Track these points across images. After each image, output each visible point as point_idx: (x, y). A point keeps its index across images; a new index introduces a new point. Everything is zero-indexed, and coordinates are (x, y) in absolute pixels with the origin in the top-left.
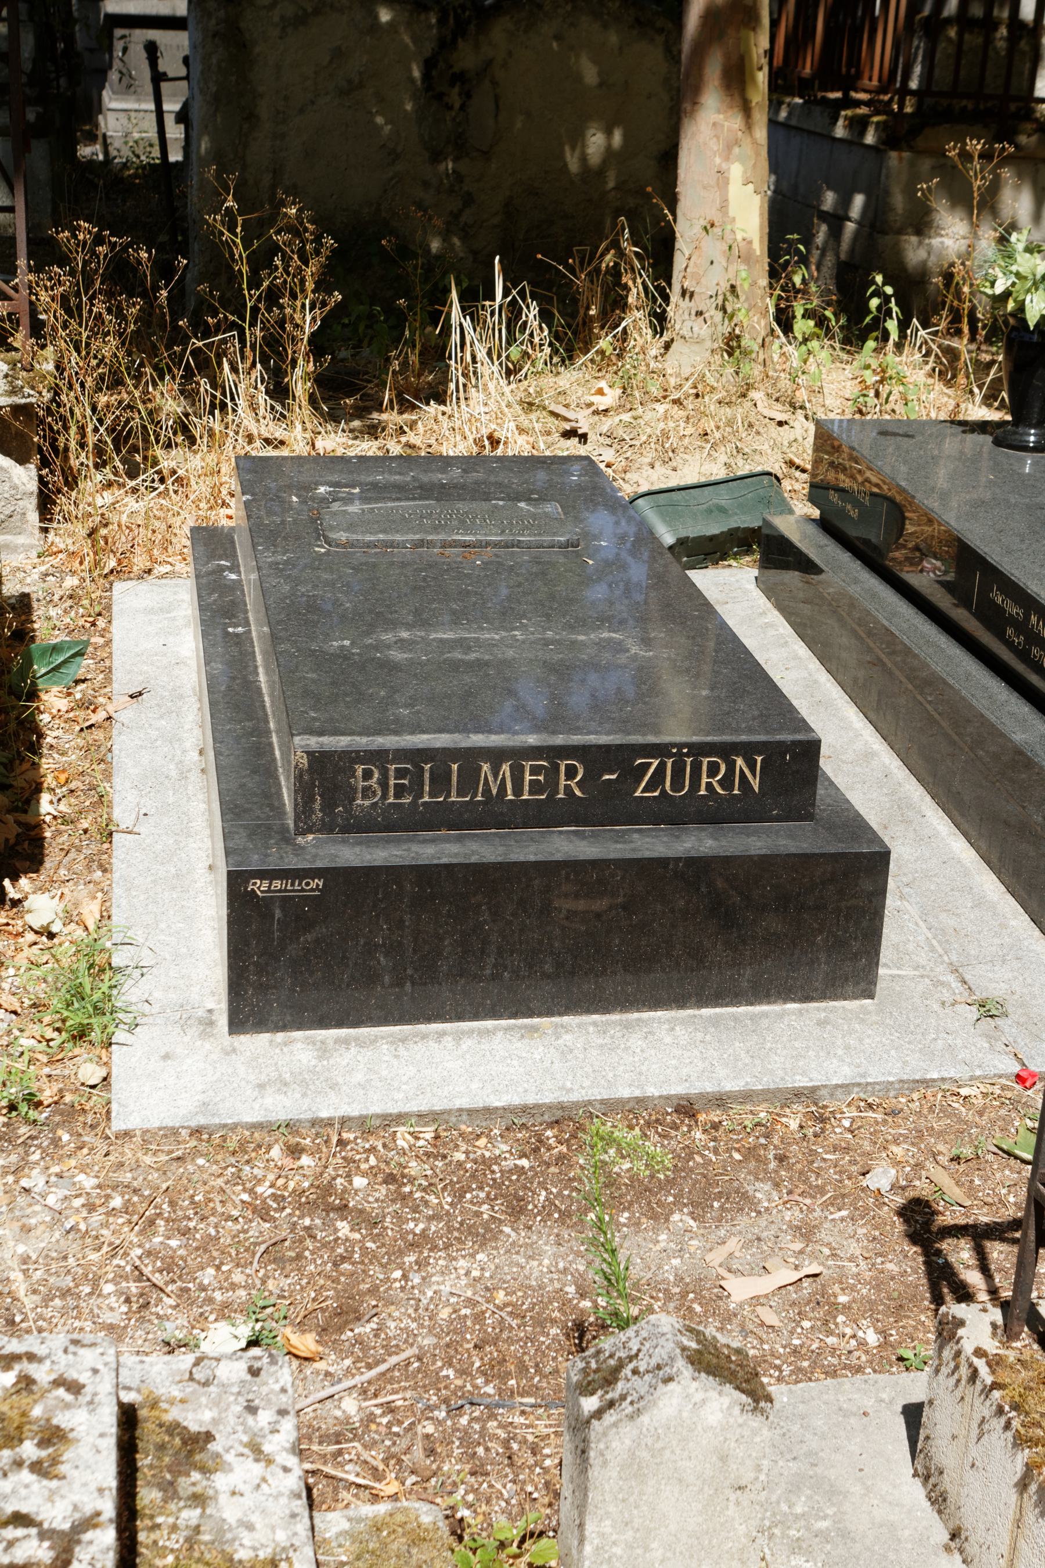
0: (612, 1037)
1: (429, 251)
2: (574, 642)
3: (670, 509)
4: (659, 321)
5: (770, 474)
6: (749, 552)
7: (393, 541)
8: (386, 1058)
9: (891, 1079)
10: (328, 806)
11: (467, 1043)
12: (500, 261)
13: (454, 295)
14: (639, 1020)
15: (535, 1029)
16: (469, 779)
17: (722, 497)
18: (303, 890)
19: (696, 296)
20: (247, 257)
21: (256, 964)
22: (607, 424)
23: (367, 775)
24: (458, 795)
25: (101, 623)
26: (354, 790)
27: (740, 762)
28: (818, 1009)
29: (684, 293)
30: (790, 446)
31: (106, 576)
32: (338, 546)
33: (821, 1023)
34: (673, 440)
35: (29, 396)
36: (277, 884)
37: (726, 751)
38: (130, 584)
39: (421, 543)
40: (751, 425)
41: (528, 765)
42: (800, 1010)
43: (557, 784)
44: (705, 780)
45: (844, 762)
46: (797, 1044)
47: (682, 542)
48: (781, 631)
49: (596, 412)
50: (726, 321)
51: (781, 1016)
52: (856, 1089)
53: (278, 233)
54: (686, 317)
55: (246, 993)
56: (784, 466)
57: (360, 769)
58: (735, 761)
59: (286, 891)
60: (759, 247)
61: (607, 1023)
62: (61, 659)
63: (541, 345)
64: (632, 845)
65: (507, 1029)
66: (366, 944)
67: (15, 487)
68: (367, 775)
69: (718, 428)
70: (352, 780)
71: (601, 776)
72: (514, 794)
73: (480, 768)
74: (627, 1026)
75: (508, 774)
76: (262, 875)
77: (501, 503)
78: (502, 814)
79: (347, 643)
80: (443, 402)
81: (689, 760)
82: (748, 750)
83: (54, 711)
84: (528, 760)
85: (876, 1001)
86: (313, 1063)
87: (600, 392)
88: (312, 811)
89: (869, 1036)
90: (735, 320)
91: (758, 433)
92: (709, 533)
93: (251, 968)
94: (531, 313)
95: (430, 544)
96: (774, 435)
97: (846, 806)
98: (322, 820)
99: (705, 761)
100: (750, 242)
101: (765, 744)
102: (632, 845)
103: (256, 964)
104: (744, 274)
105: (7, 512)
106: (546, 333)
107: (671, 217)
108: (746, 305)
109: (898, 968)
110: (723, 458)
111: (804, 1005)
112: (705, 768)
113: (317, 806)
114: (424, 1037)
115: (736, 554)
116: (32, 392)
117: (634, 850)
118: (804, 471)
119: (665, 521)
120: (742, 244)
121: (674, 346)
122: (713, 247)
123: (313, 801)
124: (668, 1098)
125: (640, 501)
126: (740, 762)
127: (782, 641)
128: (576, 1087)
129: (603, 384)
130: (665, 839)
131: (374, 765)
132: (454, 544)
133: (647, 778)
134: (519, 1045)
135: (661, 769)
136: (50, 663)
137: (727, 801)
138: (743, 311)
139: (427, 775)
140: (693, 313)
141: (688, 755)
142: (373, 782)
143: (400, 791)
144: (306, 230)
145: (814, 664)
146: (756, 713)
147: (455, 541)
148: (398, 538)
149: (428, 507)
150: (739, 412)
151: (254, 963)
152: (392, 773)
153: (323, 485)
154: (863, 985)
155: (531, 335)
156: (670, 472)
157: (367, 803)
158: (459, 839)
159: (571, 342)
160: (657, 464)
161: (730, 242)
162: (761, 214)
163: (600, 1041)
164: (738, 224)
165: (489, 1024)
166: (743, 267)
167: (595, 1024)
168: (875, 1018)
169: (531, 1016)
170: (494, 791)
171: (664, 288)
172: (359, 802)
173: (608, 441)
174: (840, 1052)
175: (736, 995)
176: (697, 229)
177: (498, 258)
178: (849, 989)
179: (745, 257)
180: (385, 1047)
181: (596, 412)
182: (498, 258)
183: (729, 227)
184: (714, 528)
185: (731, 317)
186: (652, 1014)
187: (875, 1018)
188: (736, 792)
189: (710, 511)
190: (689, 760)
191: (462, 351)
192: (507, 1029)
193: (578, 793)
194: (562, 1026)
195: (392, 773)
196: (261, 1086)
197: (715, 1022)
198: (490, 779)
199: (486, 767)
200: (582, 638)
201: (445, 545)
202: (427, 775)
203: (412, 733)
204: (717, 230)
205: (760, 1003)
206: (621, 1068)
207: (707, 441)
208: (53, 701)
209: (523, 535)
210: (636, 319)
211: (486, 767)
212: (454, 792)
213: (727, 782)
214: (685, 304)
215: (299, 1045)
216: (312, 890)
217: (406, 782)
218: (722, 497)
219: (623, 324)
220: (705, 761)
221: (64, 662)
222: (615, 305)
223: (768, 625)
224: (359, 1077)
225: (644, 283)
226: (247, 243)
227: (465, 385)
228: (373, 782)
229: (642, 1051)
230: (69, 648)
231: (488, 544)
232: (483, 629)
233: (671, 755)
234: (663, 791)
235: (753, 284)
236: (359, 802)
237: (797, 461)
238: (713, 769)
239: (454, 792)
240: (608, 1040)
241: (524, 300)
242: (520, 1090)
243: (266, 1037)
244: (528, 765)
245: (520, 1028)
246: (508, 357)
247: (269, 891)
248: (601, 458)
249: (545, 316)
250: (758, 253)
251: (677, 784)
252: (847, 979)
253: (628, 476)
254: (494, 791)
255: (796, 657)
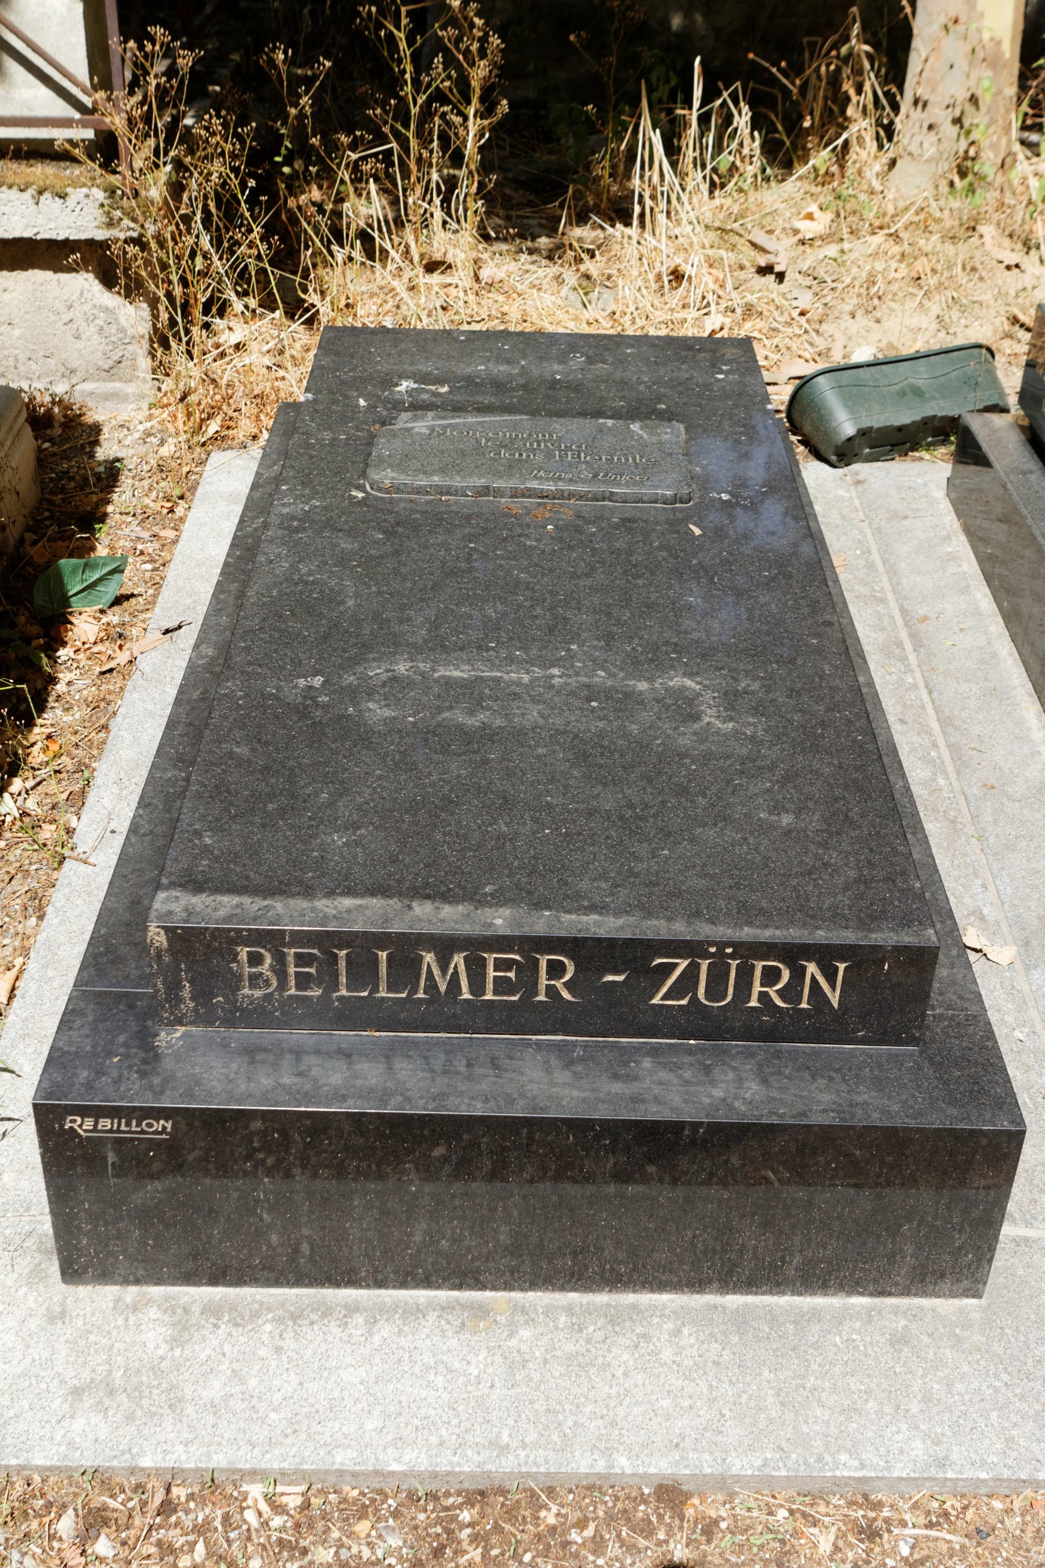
0: (588, 1341)
1: (669, 27)
2: (628, 695)
3: (854, 390)
4: (887, 132)
5: (980, 346)
6: (945, 442)
7: (450, 487)
8: (263, 1352)
9: (983, 1475)
10: (202, 996)
11: (385, 1330)
12: (702, 63)
13: (644, 103)
14: (634, 1307)
15: (482, 1311)
16: (405, 968)
17: (920, 376)
18: (143, 1132)
19: (929, 106)
20: (412, 55)
21: (88, 1212)
22: (811, 258)
23: (255, 960)
24: (389, 990)
25: (180, 511)
26: (240, 978)
27: (812, 968)
28: (896, 1310)
29: (916, 102)
30: (1017, 296)
31: (204, 444)
32: (380, 490)
33: (898, 1341)
34: (880, 283)
35: (129, 229)
36: (105, 1123)
37: (793, 954)
38: (230, 454)
39: (486, 491)
40: (974, 269)
41: (491, 958)
42: (870, 1310)
43: (536, 984)
44: (757, 988)
45: (1010, 798)
46: (854, 1383)
47: (863, 433)
48: (965, 567)
49: (802, 242)
50: (962, 138)
51: (841, 1318)
52: (927, 1484)
53: (443, 28)
54: (916, 129)
55: (79, 1242)
56: (1006, 322)
57: (243, 953)
58: (804, 968)
59: (118, 1131)
60: (1010, 49)
61: (588, 1311)
62: (96, 576)
63: (752, 156)
64: (635, 1087)
65: (446, 1308)
66: (239, 1198)
67: (123, 330)
68: (255, 960)
69: (934, 271)
70: (234, 965)
71: (600, 978)
72: (472, 993)
73: (421, 959)
74: (614, 1318)
75: (462, 968)
76: (83, 1111)
77: (610, 422)
78: (454, 1015)
79: (318, 681)
80: (628, 224)
81: (734, 964)
82: (826, 956)
83: (79, 644)
84: (491, 950)
85: (983, 1301)
86: (160, 1352)
87: (810, 217)
88: (180, 1000)
89: (963, 1377)
90: (972, 138)
91: (981, 279)
92: (897, 423)
93: (82, 1215)
94: (742, 120)
95: (498, 493)
96: (1000, 282)
97: (974, 1009)
98: (195, 1010)
99: (759, 965)
100: (999, 43)
101: (852, 947)
102: (635, 1087)
103: (88, 1212)
104: (986, 83)
105: (116, 358)
106: (757, 143)
107: (908, 10)
108: (986, 120)
109: (1029, 1224)
110: (935, 309)
111: (878, 1301)
112: (758, 973)
113: (186, 992)
114: (326, 1311)
115: (929, 445)
116: (132, 225)
117: (637, 1099)
118: (1028, 330)
119: (846, 406)
120: (989, 46)
121: (899, 163)
122: (954, 48)
123: (179, 986)
124: (645, 1476)
125: (820, 379)
126: (812, 968)
127: (963, 584)
128: (514, 1444)
129: (813, 208)
130: (688, 1075)
131: (264, 947)
132: (529, 493)
133: (669, 982)
134: (453, 1342)
135: (690, 977)
136: (82, 581)
137: (791, 1017)
138: (982, 127)
139: (342, 964)
140: (926, 126)
141: (732, 956)
142: (265, 968)
143: (303, 982)
144: (472, 26)
145: (997, 626)
146: (853, 874)
147: (529, 489)
148: (457, 482)
149: (515, 426)
150: (962, 251)
151: (86, 1211)
152: (291, 959)
153: (407, 378)
154: (966, 1284)
155: (741, 145)
156: (872, 324)
157: (258, 993)
158: (389, 1053)
159: (782, 155)
160: (859, 314)
161: (975, 42)
162: (1016, 9)
163: (569, 1347)
164: (987, 22)
165: (422, 1295)
166: (989, 73)
167: (569, 1310)
168: (977, 1338)
169: (483, 1287)
170: (443, 988)
171: (894, 95)
172: (246, 991)
173: (809, 281)
174: (915, 1408)
175: (778, 1284)
176: (936, 28)
177: (698, 59)
178: (946, 1285)
179: (993, 62)
180: (268, 1327)
181: (802, 242)
182: (698, 59)
183: (973, 26)
184: (905, 416)
185: (968, 133)
186: (655, 1297)
187: (977, 1338)
188: (804, 1005)
189: (902, 394)
190: (734, 964)
191: (650, 168)
192: (446, 1308)
193: (566, 995)
194: (524, 1311)
195: (291, 959)
196: (77, 1392)
197: (741, 1320)
198: (436, 972)
199: (429, 958)
200: (643, 686)
201: (515, 494)
202: (342, 964)
203: (331, 894)
204: (960, 28)
205: (813, 1294)
206: (588, 1409)
207: (920, 287)
208: (84, 627)
209: (619, 485)
210: (860, 127)
211: (429, 958)
212: (383, 985)
213: (791, 993)
214: (917, 114)
215: (153, 1313)
216: (156, 1132)
217: (312, 970)
218: (920, 376)
219: (844, 136)
220: (759, 965)
221: (100, 580)
222: (835, 117)
223: (952, 557)
224: (215, 1389)
225: (873, 86)
226: (410, 42)
227: (652, 209)
228: (265, 968)
229: (626, 1374)
230: (105, 564)
231: (571, 495)
232: (511, 659)
233: (706, 955)
234: (695, 1000)
235: (999, 93)
236: (246, 991)
237: (1022, 318)
238: (771, 976)
239: (383, 985)
240: (581, 1347)
241: (736, 103)
242: (434, 1440)
243: (110, 1291)
244: (491, 958)
245: (464, 1307)
246: (714, 170)
247: (95, 1129)
248: (795, 303)
249: (756, 124)
250: (1007, 55)
251: (715, 989)
252: (942, 1276)
253: (823, 327)
254: (443, 988)
255: (977, 613)
